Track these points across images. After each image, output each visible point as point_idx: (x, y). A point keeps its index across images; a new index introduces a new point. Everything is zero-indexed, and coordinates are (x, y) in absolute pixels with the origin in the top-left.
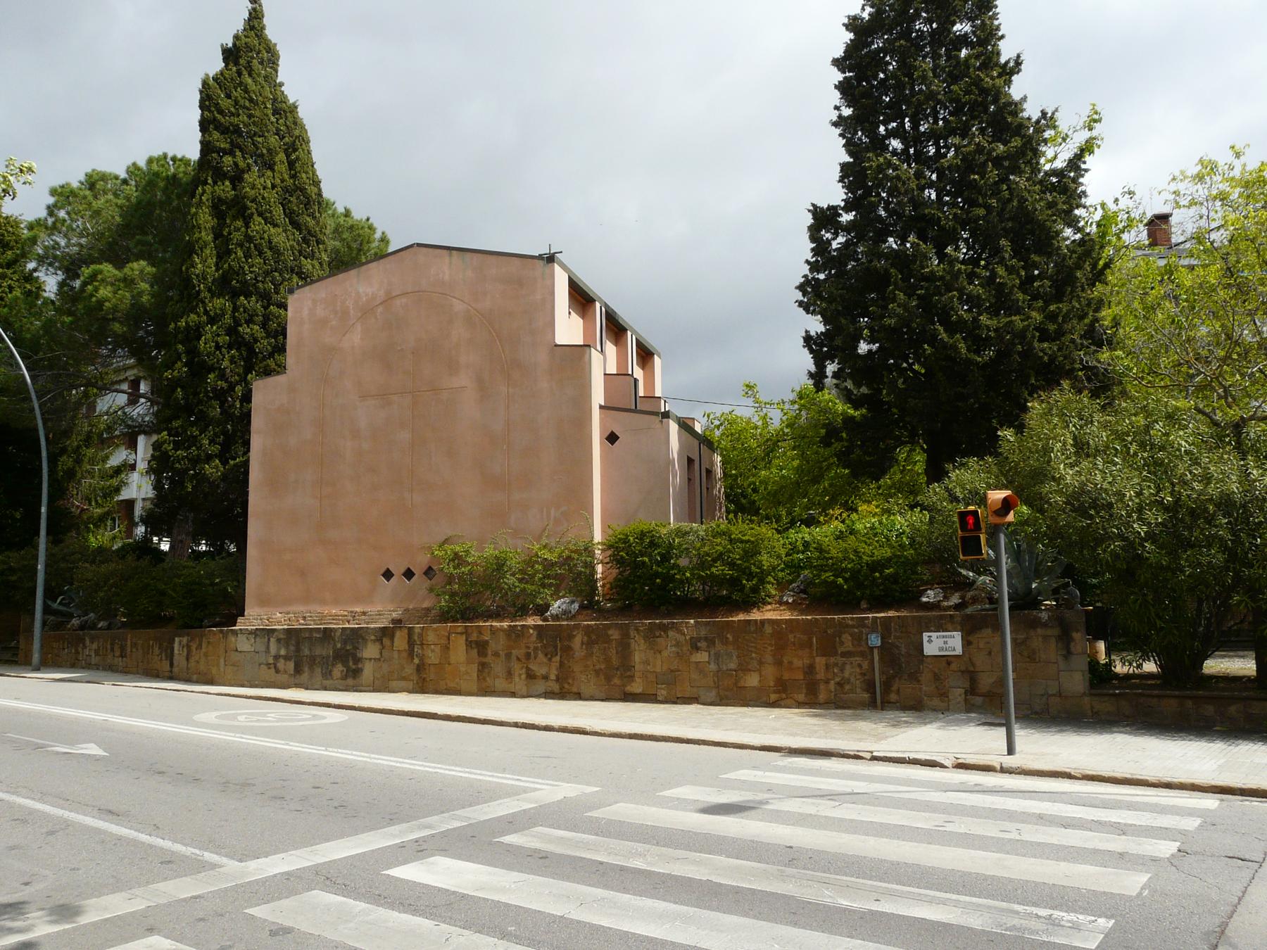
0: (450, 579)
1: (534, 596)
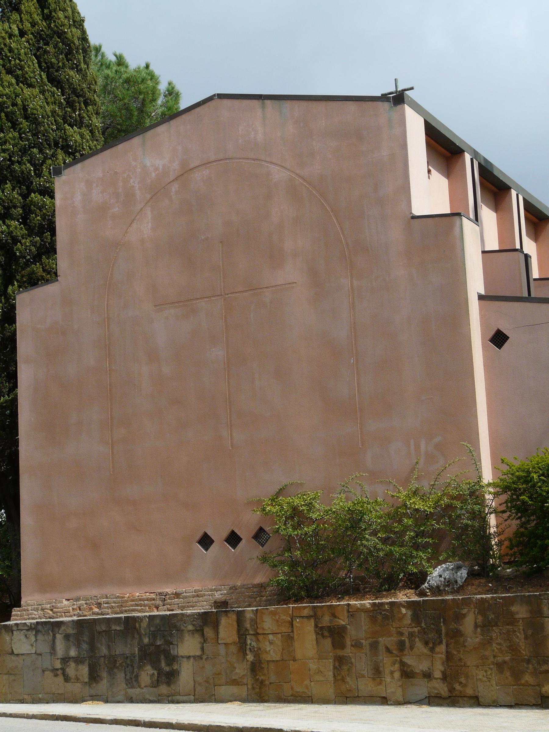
0: (289, 544)
1: (405, 560)
